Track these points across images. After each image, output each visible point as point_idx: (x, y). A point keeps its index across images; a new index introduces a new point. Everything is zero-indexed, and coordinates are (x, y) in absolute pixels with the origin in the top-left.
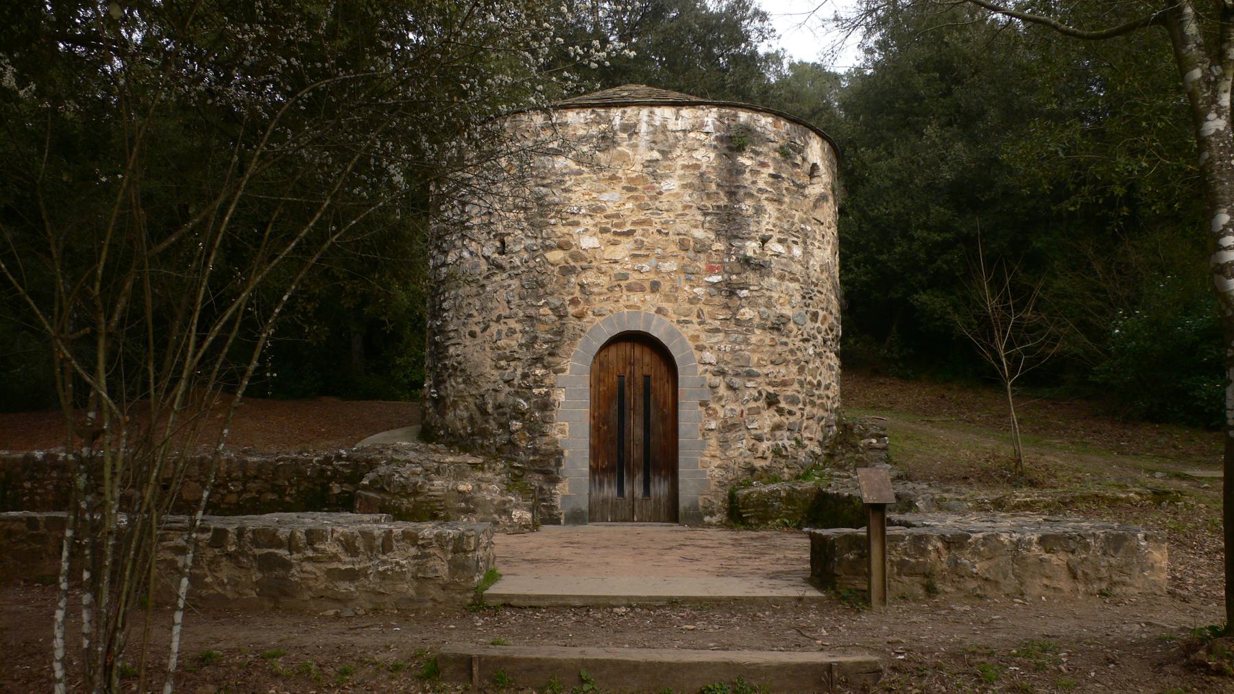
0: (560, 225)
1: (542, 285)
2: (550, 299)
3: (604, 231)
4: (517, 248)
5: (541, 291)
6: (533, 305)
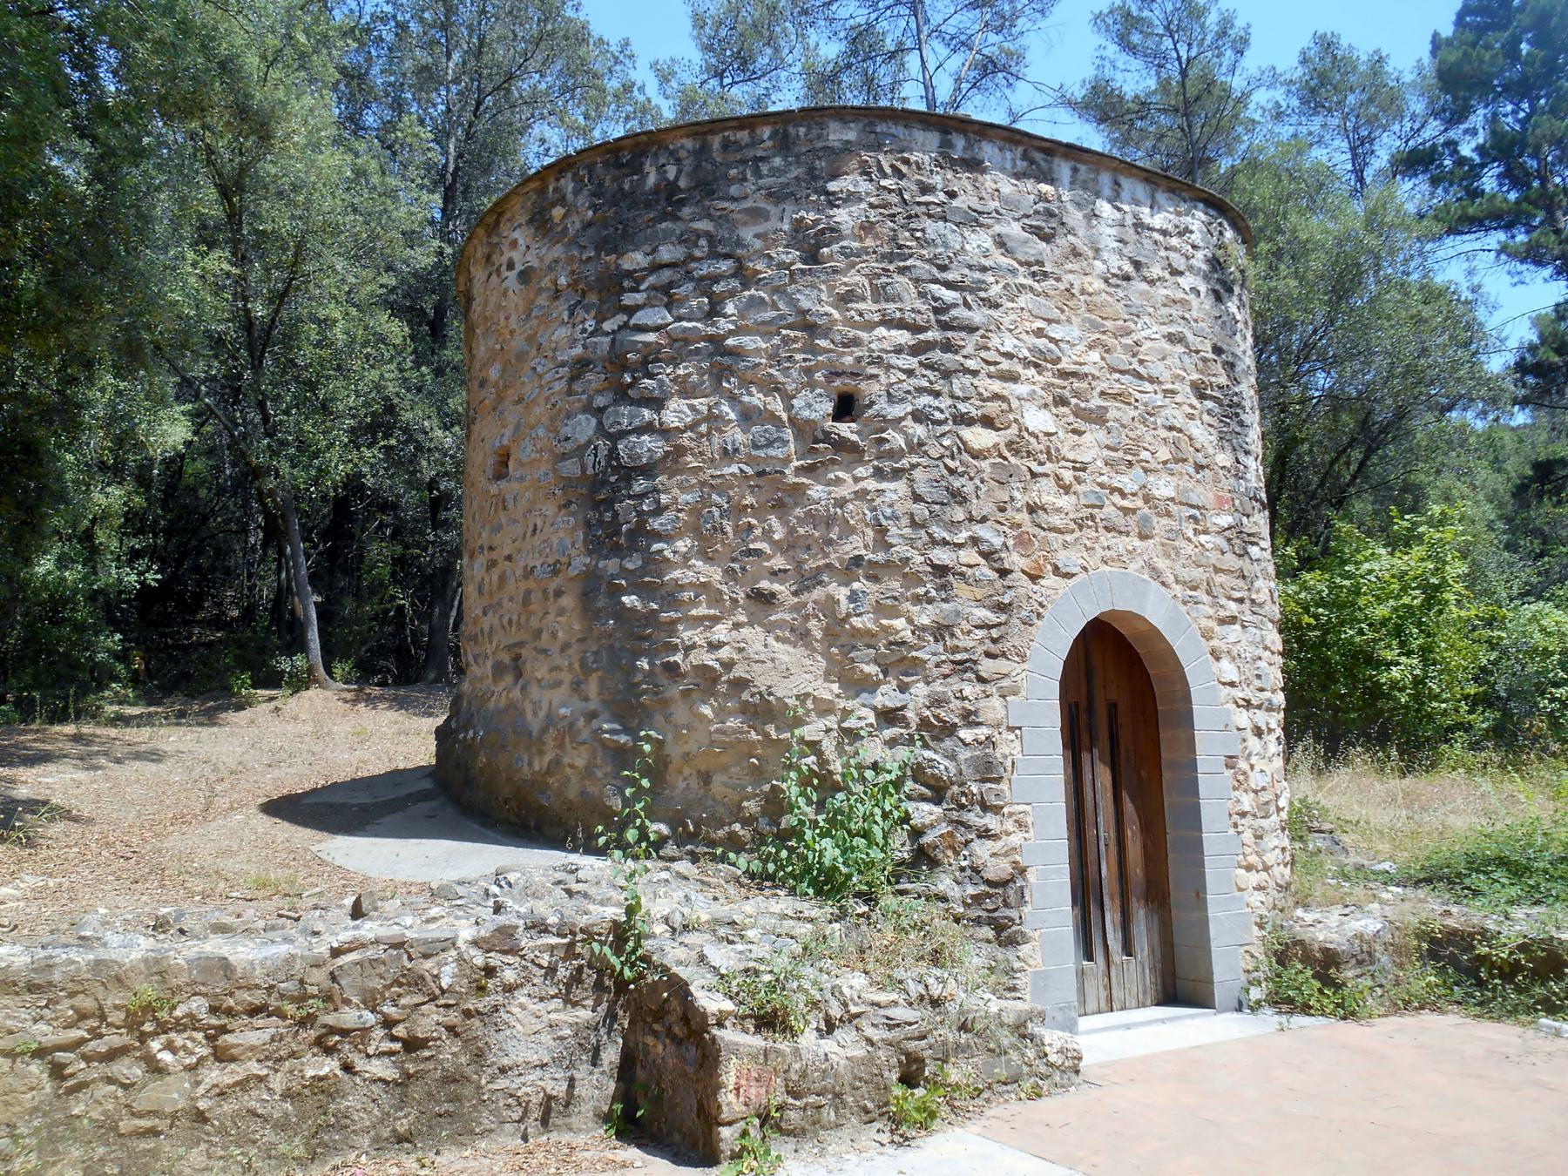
0: (983, 374)
1: (958, 497)
2: (982, 531)
3: (1061, 401)
4: (896, 411)
5: (959, 514)
6: (945, 543)
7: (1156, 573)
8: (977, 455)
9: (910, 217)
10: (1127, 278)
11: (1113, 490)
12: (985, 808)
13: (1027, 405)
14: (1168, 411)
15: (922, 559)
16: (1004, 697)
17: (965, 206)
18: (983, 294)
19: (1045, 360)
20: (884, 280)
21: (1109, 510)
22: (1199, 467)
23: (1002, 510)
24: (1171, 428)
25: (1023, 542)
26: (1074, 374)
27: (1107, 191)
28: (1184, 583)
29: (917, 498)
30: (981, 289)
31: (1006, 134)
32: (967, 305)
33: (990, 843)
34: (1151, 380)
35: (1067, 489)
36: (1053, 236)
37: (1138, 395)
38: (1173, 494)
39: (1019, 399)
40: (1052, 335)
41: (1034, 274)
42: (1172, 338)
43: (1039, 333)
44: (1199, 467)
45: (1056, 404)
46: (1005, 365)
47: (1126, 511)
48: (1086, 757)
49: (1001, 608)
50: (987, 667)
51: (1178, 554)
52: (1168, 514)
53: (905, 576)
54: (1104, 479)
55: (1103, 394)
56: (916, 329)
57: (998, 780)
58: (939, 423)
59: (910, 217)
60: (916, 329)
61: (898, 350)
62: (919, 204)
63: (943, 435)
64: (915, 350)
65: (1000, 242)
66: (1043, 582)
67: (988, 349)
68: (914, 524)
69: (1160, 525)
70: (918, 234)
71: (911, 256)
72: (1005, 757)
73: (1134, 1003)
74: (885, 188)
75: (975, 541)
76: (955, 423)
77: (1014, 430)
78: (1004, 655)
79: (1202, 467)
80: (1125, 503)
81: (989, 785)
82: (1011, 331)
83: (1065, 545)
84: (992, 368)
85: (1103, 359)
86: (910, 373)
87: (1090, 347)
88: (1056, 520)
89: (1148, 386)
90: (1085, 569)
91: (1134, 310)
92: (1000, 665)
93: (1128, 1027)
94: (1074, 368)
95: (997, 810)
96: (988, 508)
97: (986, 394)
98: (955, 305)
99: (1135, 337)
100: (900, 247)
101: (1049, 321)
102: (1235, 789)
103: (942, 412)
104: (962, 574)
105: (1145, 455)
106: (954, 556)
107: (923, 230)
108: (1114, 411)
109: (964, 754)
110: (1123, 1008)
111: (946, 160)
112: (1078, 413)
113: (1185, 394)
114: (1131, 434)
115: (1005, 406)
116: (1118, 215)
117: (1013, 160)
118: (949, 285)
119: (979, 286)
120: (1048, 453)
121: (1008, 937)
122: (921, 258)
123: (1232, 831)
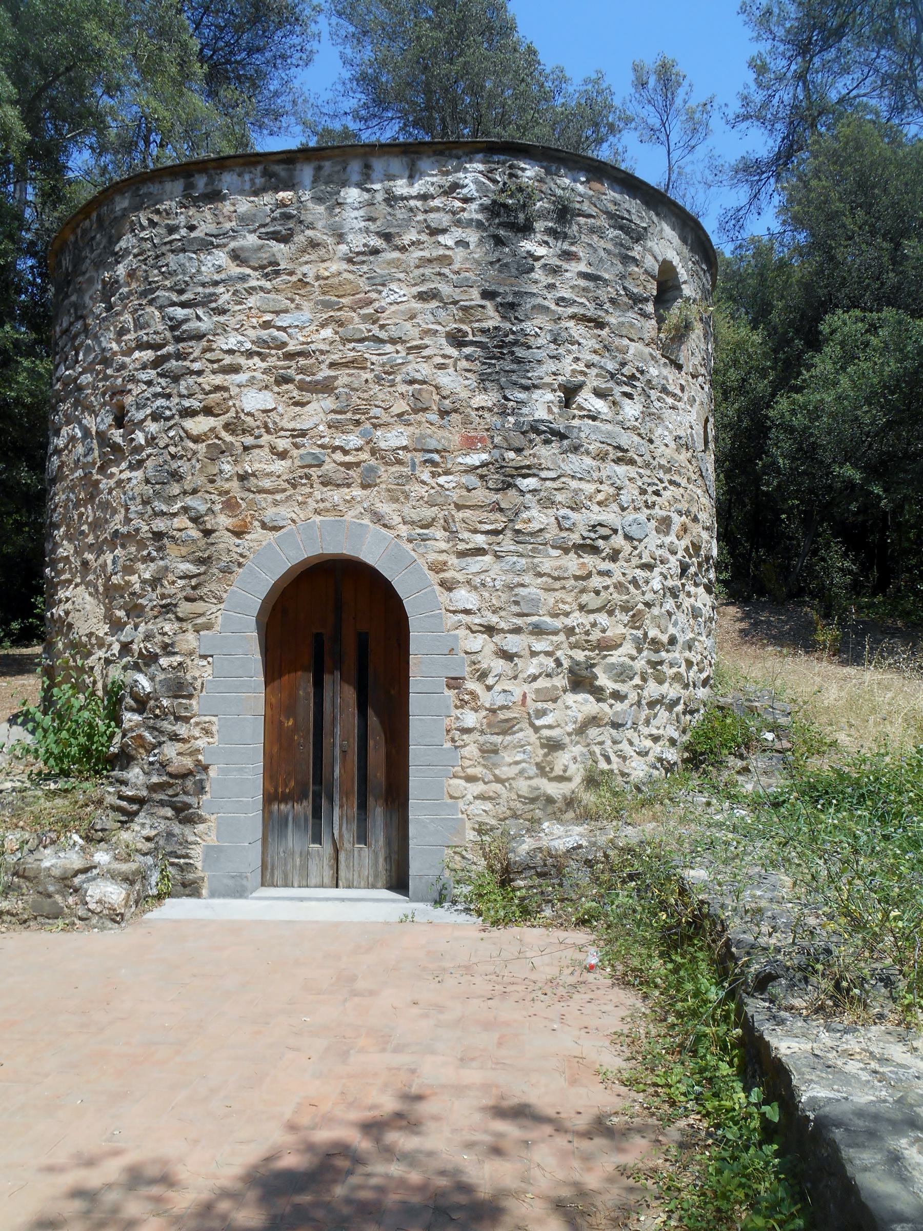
1: (176, 476)
2: (190, 501)
5: (175, 489)
6: (163, 514)
7: (378, 518)
8: (196, 440)
9: (157, 257)
10: (375, 252)
11: (335, 449)
12: (178, 718)
13: (245, 390)
14: (410, 368)
15: (147, 528)
16: (198, 632)
17: (202, 235)
18: (213, 305)
19: (269, 348)
20: (140, 312)
21: (329, 466)
22: (443, 413)
23: (212, 481)
24: (412, 382)
25: (230, 506)
26: (300, 354)
27: (355, 177)
28: (413, 523)
29: (147, 481)
30: (211, 302)
31: (241, 161)
32: (199, 318)
33: (179, 745)
34: (393, 341)
35: (283, 455)
36: (291, 235)
37: (374, 358)
38: (405, 443)
39: (239, 386)
40: (279, 324)
41: (266, 276)
42: (422, 297)
43: (266, 325)
44: (443, 413)
45: (278, 383)
46: (228, 360)
47: (348, 466)
48: (327, 678)
49: (201, 561)
50: (185, 608)
51: (407, 497)
52: (399, 462)
53: (138, 542)
54: (326, 440)
55: (332, 365)
56: (156, 347)
57: (190, 696)
58: (168, 419)
59: (157, 257)
60: (156, 347)
61: (144, 367)
62: (165, 244)
63: (170, 428)
64: (156, 363)
65: (236, 256)
66: (247, 537)
67: (214, 350)
68: (145, 503)
69: (386, 474)
70: (163, 269)
71: (158, 288)
72: (195, 679)
73: (362, 884)
74: (142, 238)
75: (185, 509)
76: (181, 417)
77: (232, 413)
78: (201, 598)
79: (447, 413)
80: (347, 459)
81: (181, 700)
82: (237, 330)
83: (276, 503)
84: (216, 366)
85: (336, 333)
86: (149, 383)
87: (323, 326)
88: (267, 483)
89: (389, 348)
90: (293, 521)
91: (378, 281)
92: (199, 606)
93: (301, 899)
94: (299, 348)
95: (186, 720)
96: (200, 480)
97: (207, 388)
98: (186, 320)
99: (376, 305)
100: (150, 283)
101: (277, 313)
102: (457, 707)
103: (170, 410)
104: (173, 537)
105: (375, 411)
106: (169, 523)
107: (167, 265)
108: (343, 378)
109: (161, 676)
110: (349, 887)
111: (191, 200)
112: (302, 386)
113: (440, 346)
114: (365, 395)
115: (226, 395)
116: (366, 196)
117: (252, 180)
118: (183, 305)
119: (213, 297)
120: (266, 426)
121: (185, 817)
122: (165, 288)
123: (448, 745)
